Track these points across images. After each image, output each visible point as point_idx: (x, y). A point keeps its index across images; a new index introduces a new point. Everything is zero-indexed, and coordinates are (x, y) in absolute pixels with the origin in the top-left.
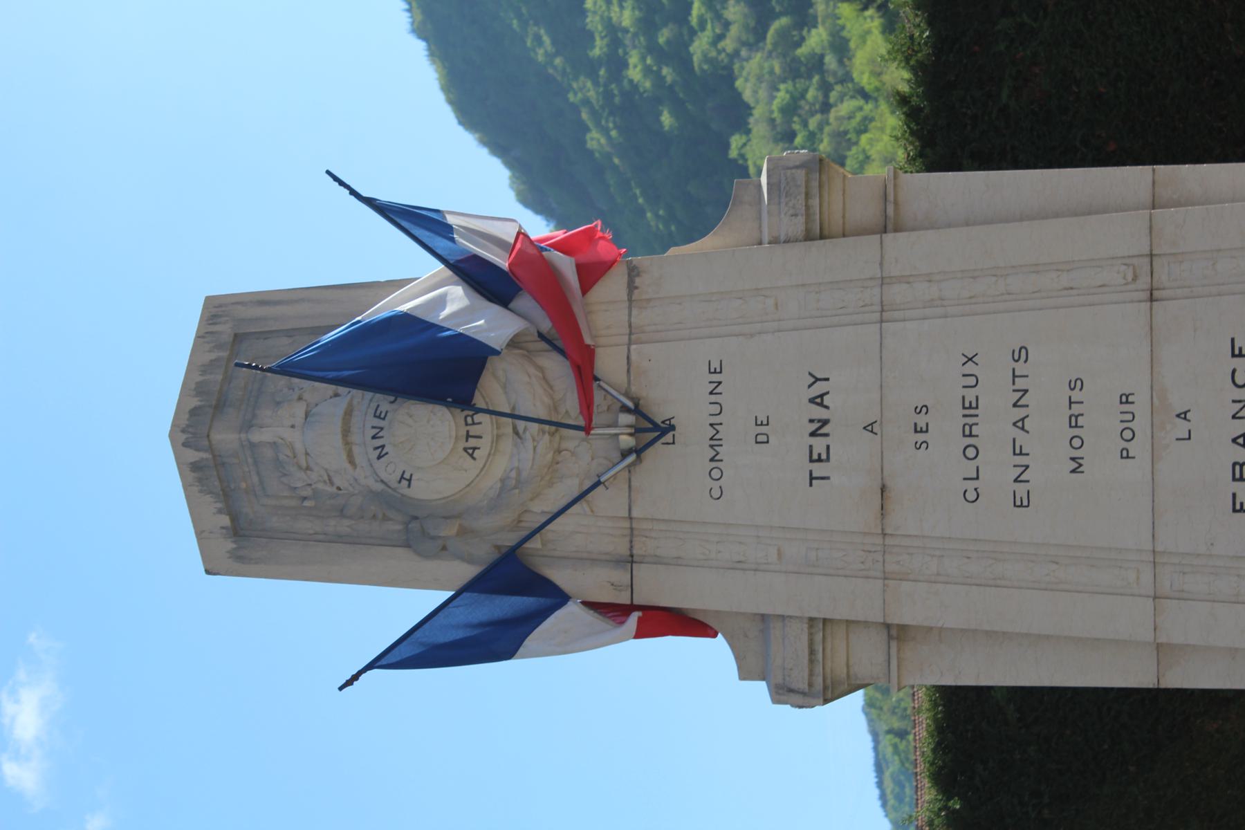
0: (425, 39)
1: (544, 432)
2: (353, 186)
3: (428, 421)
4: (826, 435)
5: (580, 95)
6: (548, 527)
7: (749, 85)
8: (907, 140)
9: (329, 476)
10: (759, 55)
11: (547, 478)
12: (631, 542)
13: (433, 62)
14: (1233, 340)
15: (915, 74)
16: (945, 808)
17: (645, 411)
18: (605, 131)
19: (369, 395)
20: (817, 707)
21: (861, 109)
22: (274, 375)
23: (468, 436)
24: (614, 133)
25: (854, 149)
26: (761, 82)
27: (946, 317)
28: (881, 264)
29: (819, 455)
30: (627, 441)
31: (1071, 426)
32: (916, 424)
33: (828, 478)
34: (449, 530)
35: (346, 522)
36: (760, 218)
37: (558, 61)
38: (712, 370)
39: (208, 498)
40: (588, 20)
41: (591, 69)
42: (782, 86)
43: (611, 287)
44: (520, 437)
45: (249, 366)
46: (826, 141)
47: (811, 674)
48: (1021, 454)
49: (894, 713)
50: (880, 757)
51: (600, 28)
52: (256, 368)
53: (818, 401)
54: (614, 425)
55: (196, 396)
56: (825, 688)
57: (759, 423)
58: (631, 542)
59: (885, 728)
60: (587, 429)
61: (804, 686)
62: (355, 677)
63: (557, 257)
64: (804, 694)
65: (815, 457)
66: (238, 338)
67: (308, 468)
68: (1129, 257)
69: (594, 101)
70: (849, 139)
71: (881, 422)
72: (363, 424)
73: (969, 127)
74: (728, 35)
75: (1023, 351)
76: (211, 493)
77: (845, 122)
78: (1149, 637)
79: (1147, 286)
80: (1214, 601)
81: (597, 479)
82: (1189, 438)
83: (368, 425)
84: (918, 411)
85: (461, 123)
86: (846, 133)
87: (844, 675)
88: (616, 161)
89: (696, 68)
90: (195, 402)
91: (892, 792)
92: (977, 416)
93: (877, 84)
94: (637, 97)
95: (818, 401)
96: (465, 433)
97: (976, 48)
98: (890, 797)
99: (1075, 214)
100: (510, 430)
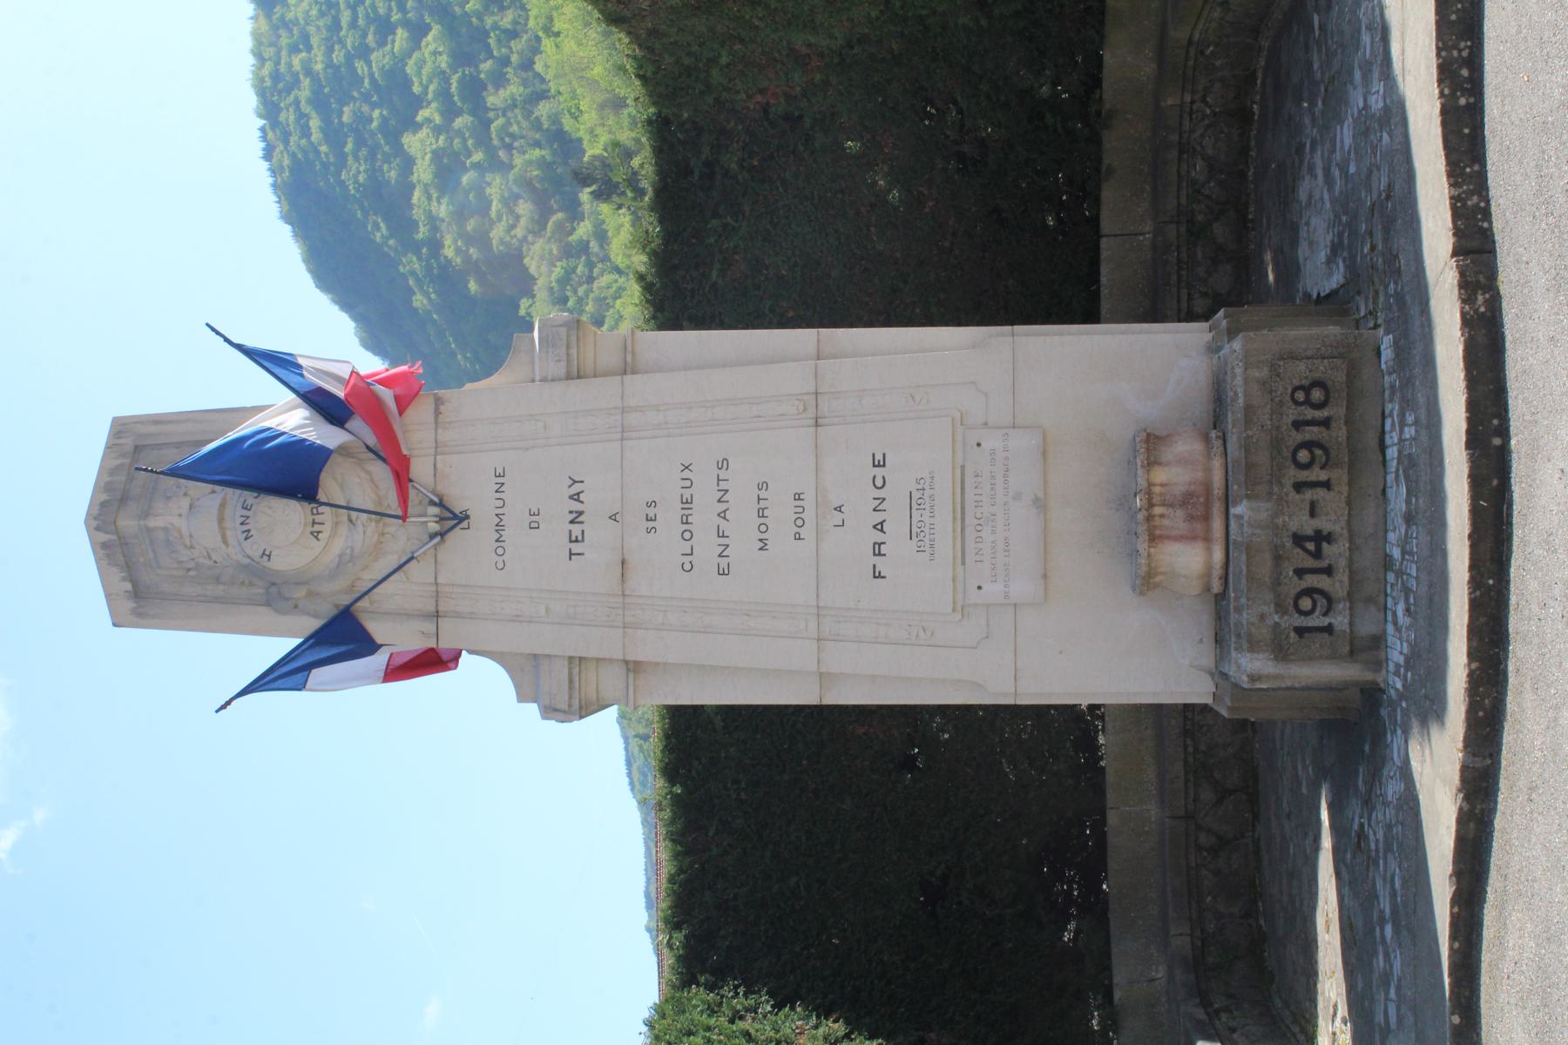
0: (290, 224)
1: (371, 520)
2: (227, 335)
3: (284, 512)
4: (582, 523)
5: (408, 268)
6: (376, 590)
7: (534, 262)
8: (644, 306)
9: (207, 552)
10: (541, 240)
11: (374, 554)
12: (437, 601)
13: (297, 241)
14: (874, 455)
15: (650, 259)
16: (671, 792)
17: (448, 505)
18: (427, 295)
19: (238, 492)
20: (575, 722)
21: (616, 281)
22: (166, 477)
23: (314, 523)
24: (433, 296)
25: (611, 310)
26: (543, 260)
27: (669, 436)
28: (622, 398)
29: (577, 537)
30: (434, 527)
31: (759, 516)
32: (647, 515)
33: (583, 554)
34: (300, 593)
35: (221, 587)
36: (533, 362)
37: (391, 242)
38: (497, 474)
39: (114, 569)
40: (414, 212)
41: (416, 248)
42: (559, 264)
43: (420, 412)
44: (354, 524)
45: (146, 470)
46: (591, 304)
47: (570, 697)
48: (723, 536)
49: (639, 722)
50: (630, 754)
51: (423, 218)
52: (152, 471)
53: (576, 497)
54: (424, 515)
55: (105, 492)
56: (581, 708)
57: (532, 513)
58: (437, 601)
59: (633, 733)
60: (404, 518)
61: (565, 706)
62: (228, 703)
63: (379, 388)
64: (565, 712)
65: (573, 538)
66: (137, 449)
67: (192, 547)
68: (801, 394)
69: (419, 273)
70: (608, 303)
71: (622, 513)
72: (234, 513)
73: (688, 298)
74: (518, 225)
75: (725, 462)
76: (117, 565)
77: (605, 290)
78: (814, 667)
79: (814, 416)
80: (860, 642)
81: (410, 555)
82: (843, 525)
83: (238, 514)
84: (649, 505)
85: (317, 287)
86: (605, 298)
87: (595, 698)
88: (435, 316)
89: (494, 247)
90: (104, 497)
91: (639, 779)
92: (691, 509)
93: (628, 263)
94: (451, 269)
95: (576, 497)
96: (311, 521)
97: (694, 241)
98: (637, 783)
99: (763, 363)
100: (346, 519)
